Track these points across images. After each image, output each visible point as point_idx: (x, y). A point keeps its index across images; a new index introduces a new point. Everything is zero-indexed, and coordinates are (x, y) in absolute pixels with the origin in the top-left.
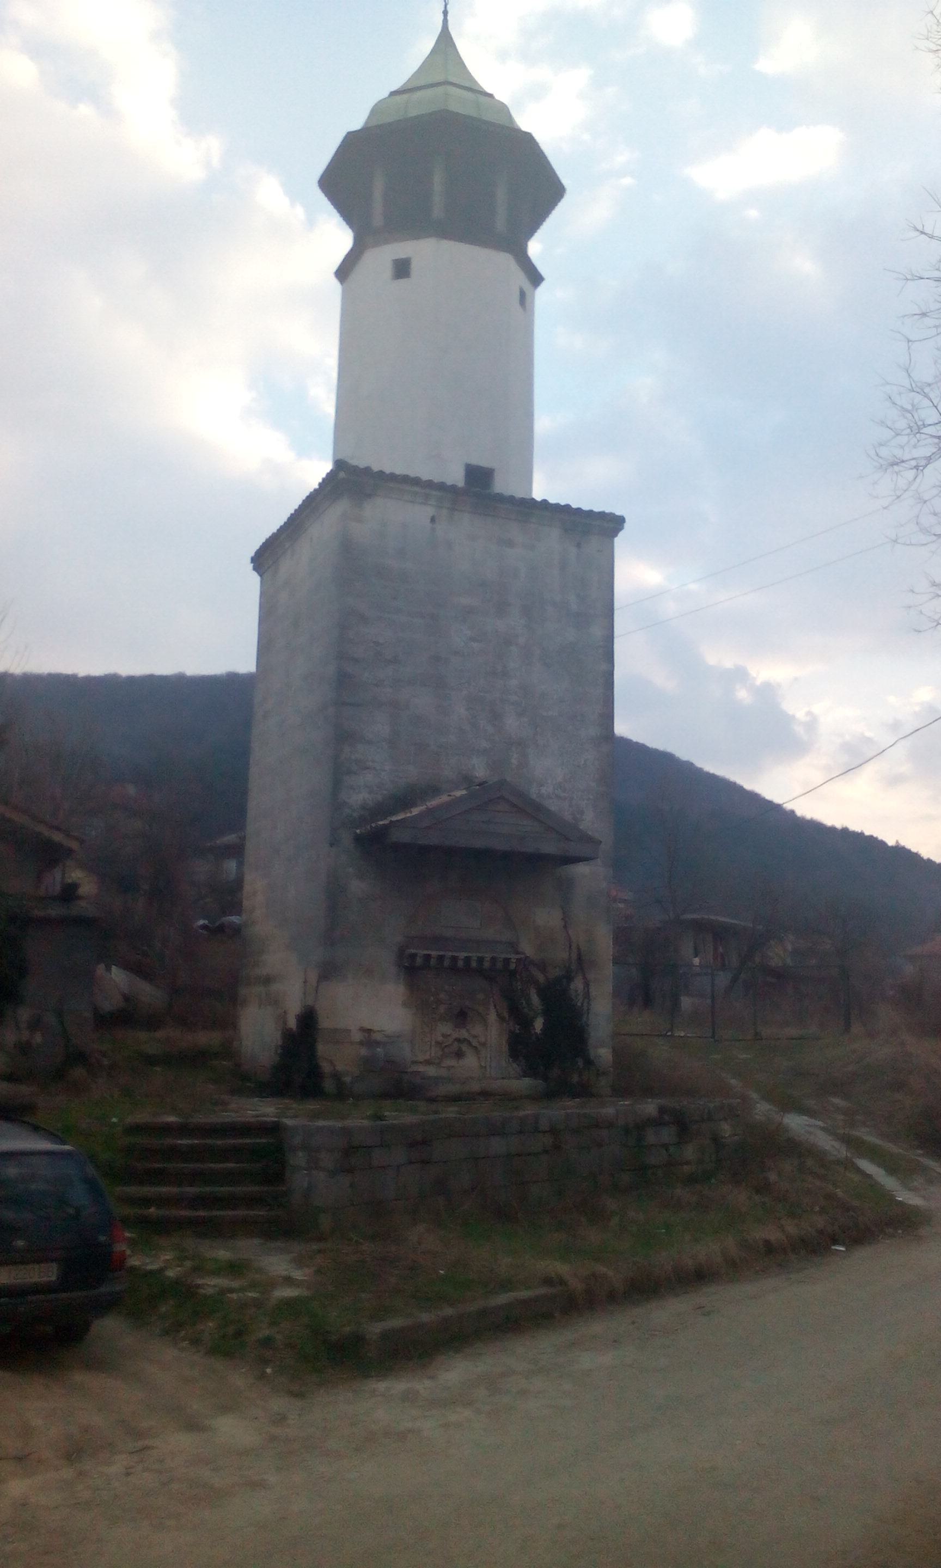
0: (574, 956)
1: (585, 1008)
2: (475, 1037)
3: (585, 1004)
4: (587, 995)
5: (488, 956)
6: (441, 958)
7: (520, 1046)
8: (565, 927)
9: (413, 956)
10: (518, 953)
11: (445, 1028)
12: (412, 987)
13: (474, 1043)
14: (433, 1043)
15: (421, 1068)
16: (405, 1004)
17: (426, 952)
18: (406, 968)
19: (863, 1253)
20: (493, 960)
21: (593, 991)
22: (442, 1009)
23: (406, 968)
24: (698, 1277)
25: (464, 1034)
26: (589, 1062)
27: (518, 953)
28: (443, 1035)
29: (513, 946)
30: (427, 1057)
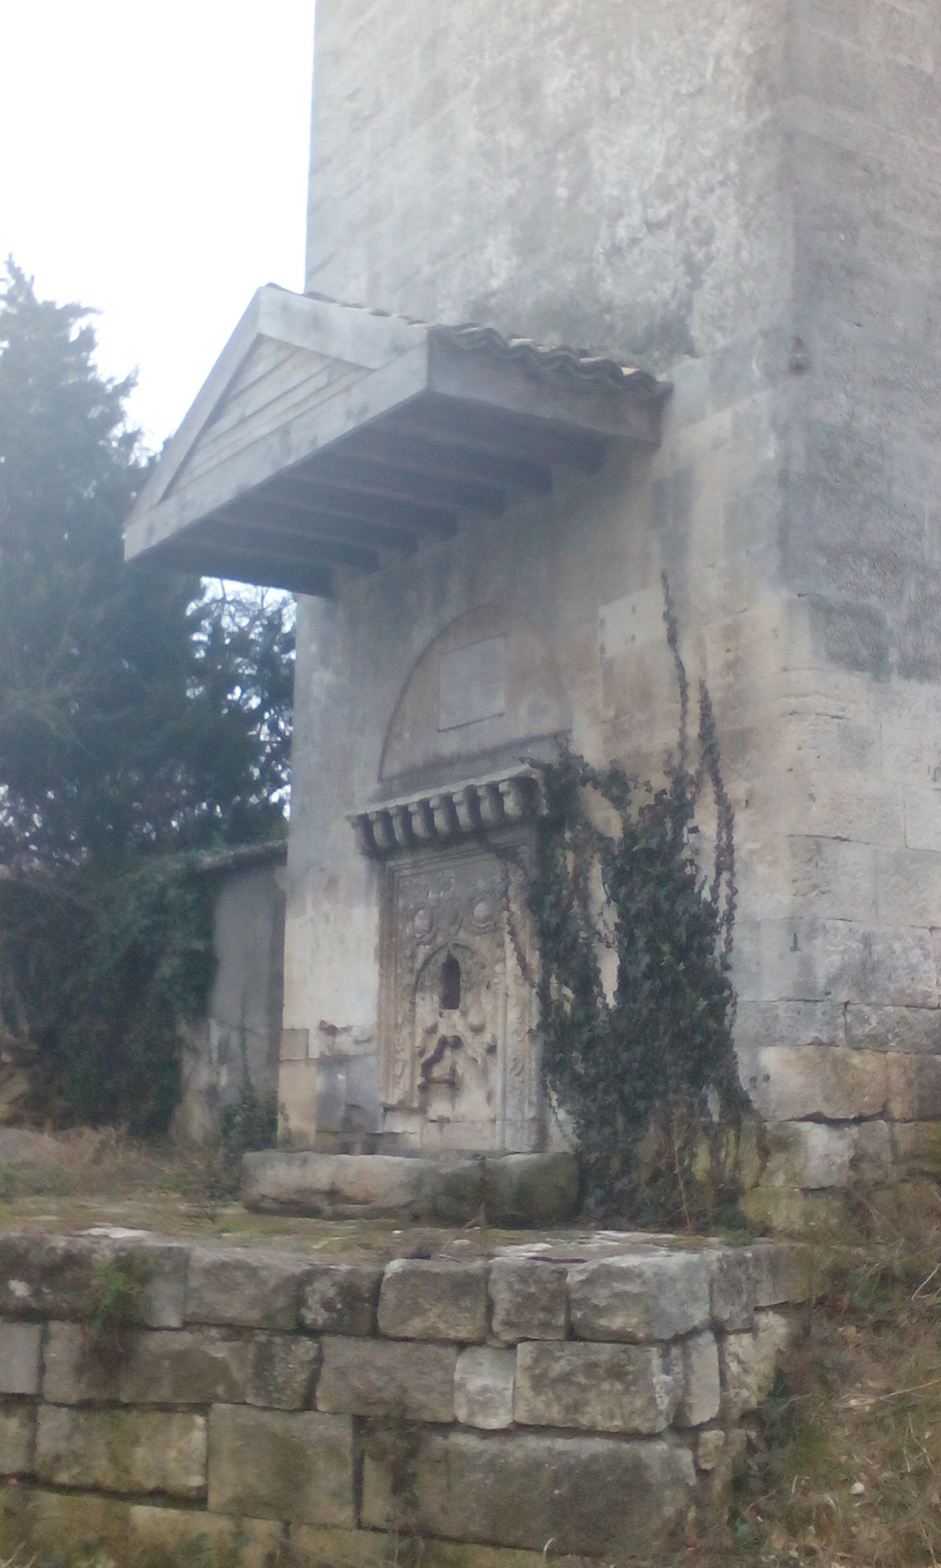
0: (693, 730)
1: (722, 906)
3: (724, 891)
4: (726, 857)
5: (457, 789)
7: (566, 1043)
20: (473, 798)
21: (745, 839)
26: (737, 1104)
29: (560, 738)
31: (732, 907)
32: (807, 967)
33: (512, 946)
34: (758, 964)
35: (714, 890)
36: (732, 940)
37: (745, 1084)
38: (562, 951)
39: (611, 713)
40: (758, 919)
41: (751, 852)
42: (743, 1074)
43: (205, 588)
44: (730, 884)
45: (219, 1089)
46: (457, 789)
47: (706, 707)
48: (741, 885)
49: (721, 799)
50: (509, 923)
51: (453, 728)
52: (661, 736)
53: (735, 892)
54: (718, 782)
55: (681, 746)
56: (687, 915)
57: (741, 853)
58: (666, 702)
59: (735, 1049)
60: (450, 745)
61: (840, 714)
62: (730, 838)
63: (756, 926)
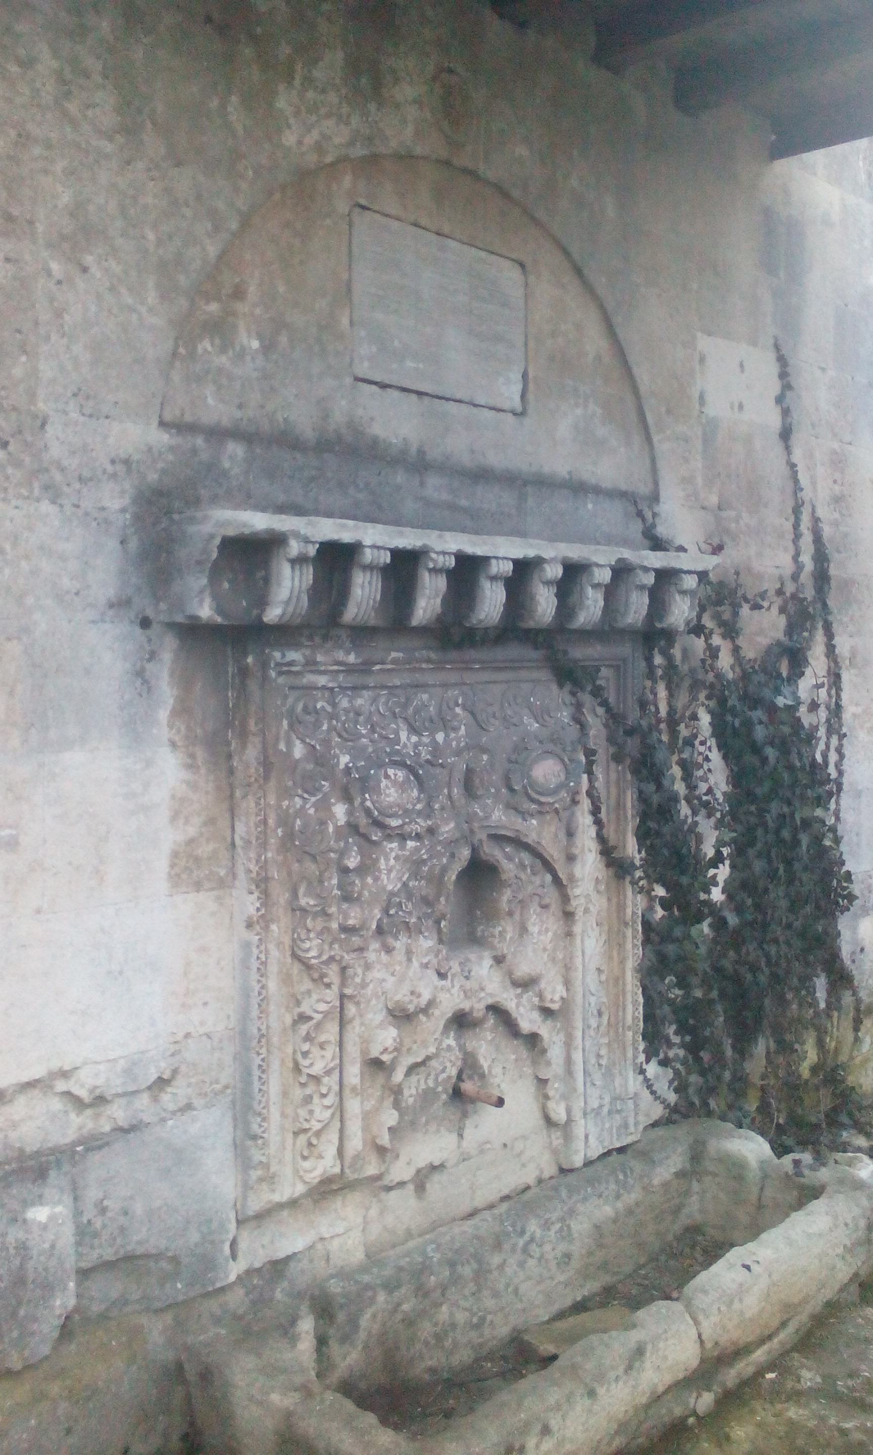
0: (807, 559)
2: (526, 984)
3: (833, 757)
5: (602, 559)
6: (403, 567)
8: (786, 434)
9: (250, 555)
10: (657, 544)
11: (406, 971)
12: (219, 741)
14: (354, 1073)
15: (290, 1239)
16: (188, 870)
17: (329, 529)
18: (192, 632)
19: (27, 1080)
22: (391, 869)
23: (192, 632)
25: (486, 981)
27: (657, 544)
29: (640, 508)
30: (327, 1163)
32: (284, 1023)
34: (857, 835)
36: (839, 810)
37: (847, 962)
38: (668, 858)
39: (714, 499)
40: (860, 787)
41: (855, 716)
42: (845, 952)
43: (723, 893)
44: (839, 751)
47: (818, 539)
49: (831, 650)
51: (404, 390)
52: (771, 560)
53: (841, 756)
55: (795, 577)
56: (408, 1259)
57: (849, 712)
58: (777, 518)
59: (839, 928)
60: (394, 423)
62: (838, 696)
63: (858, 794)
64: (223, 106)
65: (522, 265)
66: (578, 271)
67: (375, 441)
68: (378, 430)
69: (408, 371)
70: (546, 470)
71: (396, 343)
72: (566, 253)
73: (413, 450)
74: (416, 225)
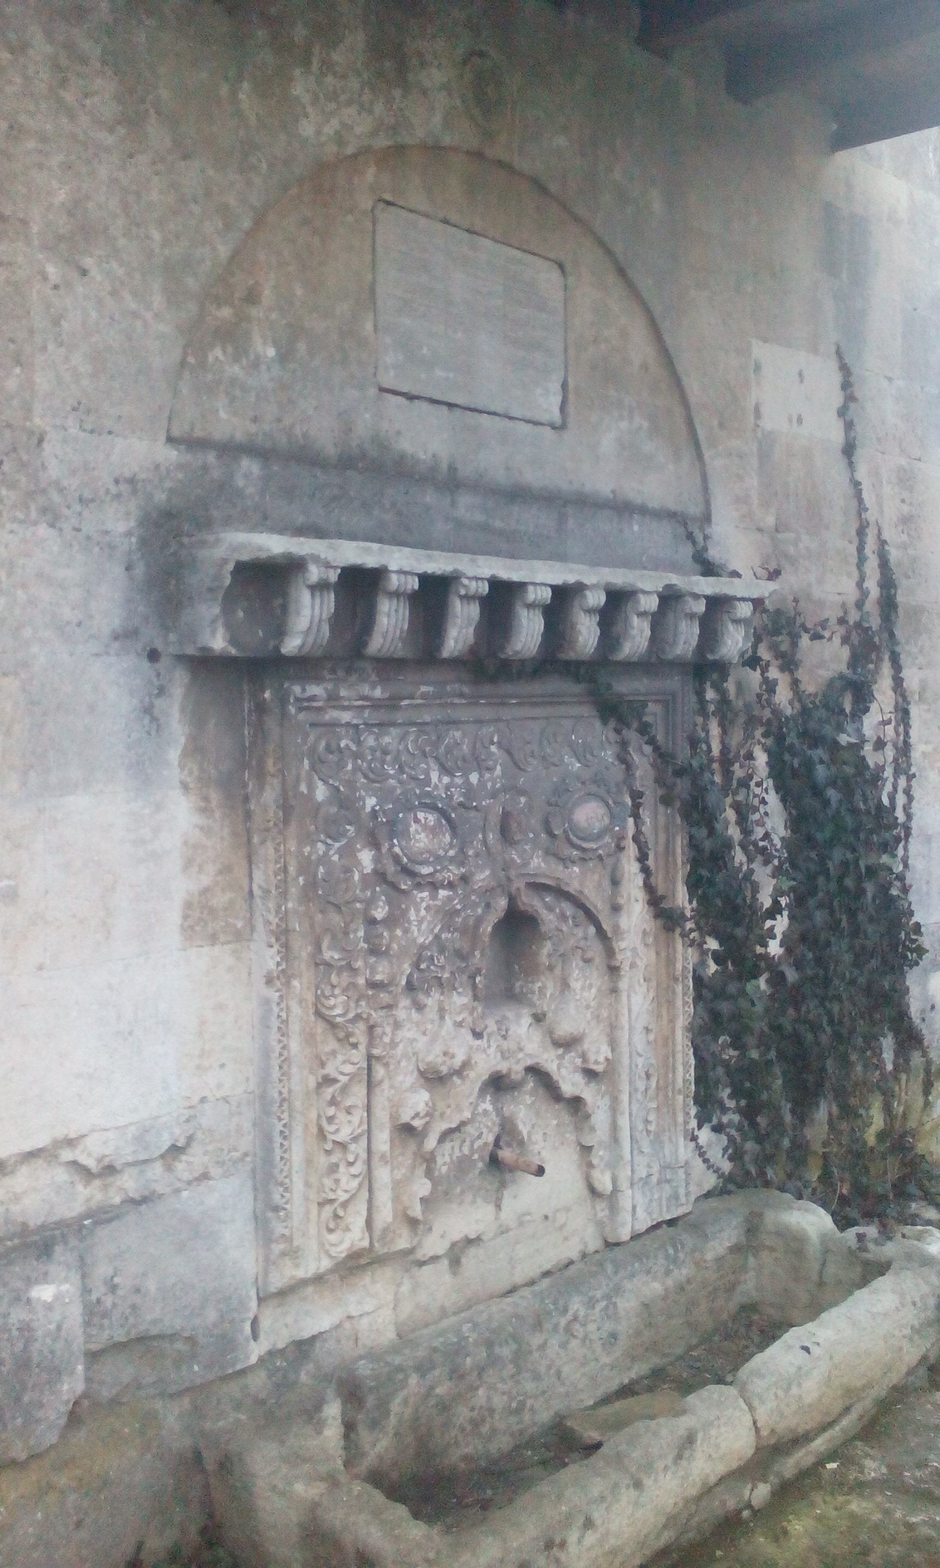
0: (874, 592)
2: (567, 1044)
3: (901, 799)
5: (649, 585)
6: (433, 594)
8: (849, 450)
9: (266, 581)
10: (709, 569)
11: (439, 1030)
12: (236, 783)
13: (571, 1083)
14: (383, 1139)
15: (317, 1318)
16: (202, 921)
18: (204, 665)
22: (421, 921)
23: (204, 665)
24: (255, 1199)
25: (525, 1041)
27: (709, 569)
28: (434, 1079)
29: (691, 530)
30: (354, 1236)
31: (909, 817)
33: (639, 880)
35: (892, 798)
37: (916, 1020)
39: (770, 521)
41: (924, 753)
42: (914, 1009)
44: (907, 792)
45: (492, 1090)
46: (649, 585)
47: (884, 564)
48: (916, 793)
50: (635, 839)
52: (833, 586)
53: (910, 798)
54: (897, 666)
55: (859, 605)
58: (839, 540)
60: (423, 437)
61: (167, 414)
62: (907, 734)
64: (234, 93)
65: (561, 266)
66: (621, 272)
67: (402, 457)
68: (405, 445)
69: (436, 380)
70: (588, 488)
71: (425, 351)
72: (609, 252)
73: (444, 466)
74: (446, 222)
